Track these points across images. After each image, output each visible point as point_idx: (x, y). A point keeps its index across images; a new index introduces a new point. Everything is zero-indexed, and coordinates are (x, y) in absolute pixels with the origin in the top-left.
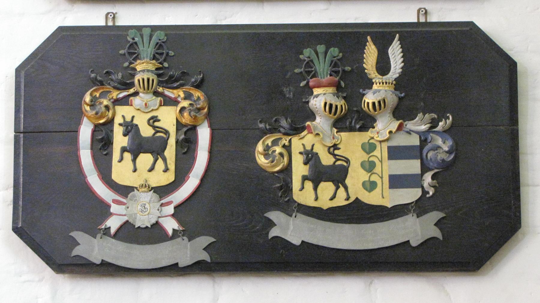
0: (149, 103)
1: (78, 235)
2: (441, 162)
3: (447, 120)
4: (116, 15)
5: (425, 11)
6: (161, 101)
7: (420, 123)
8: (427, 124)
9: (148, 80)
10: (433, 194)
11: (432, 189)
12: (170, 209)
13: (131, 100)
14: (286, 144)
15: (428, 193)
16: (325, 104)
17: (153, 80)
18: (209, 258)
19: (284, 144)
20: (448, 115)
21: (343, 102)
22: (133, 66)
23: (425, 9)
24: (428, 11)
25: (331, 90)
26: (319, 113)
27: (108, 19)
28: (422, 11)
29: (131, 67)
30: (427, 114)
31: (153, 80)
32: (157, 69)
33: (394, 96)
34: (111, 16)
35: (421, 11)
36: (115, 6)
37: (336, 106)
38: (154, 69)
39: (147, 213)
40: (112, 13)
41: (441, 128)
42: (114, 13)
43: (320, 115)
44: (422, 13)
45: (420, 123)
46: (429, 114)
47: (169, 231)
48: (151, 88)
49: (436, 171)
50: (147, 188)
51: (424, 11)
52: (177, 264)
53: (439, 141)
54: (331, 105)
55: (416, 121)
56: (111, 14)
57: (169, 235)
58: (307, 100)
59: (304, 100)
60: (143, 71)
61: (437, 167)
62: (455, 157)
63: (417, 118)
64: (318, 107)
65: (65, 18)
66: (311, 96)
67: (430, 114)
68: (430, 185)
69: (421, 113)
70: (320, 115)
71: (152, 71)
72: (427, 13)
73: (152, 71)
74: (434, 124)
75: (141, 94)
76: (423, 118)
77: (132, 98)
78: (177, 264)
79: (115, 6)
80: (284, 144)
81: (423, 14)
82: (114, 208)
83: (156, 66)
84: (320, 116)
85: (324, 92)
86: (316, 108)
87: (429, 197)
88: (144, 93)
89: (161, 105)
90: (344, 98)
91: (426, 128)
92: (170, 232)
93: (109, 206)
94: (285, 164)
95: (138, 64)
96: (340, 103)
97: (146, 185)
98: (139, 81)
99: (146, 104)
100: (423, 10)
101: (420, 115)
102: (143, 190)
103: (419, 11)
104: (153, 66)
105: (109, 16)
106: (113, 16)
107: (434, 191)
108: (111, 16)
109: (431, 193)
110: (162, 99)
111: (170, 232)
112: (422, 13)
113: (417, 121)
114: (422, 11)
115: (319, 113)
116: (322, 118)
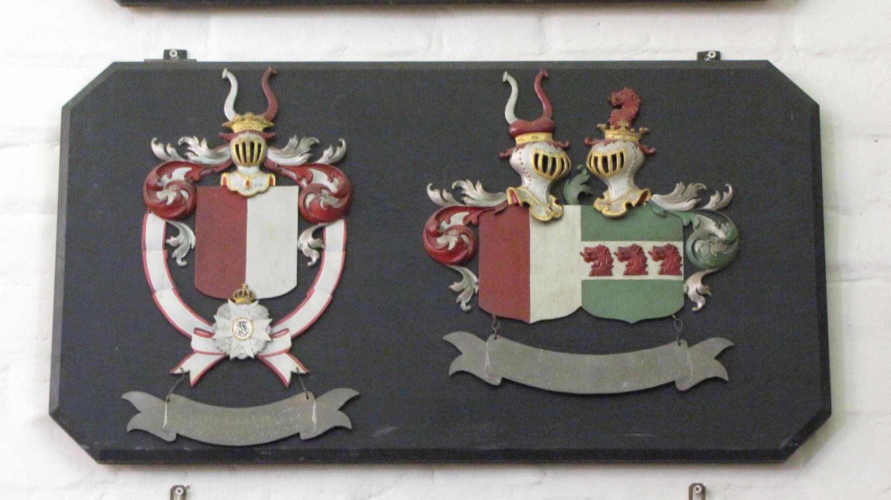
0: (253, 182)
1: (136, 397)
2: (716, 256)
3: (725, 194)
4: (188, 491)
5: (702, 488)
6: (271, 180)
7: (293, 152)
8: (691, 199)
9: (252, 145)
10: (704, 307)
11: (703, 298)
12: (285, 342)
13: (225, 179)
14: (472, 222)
15: (695, 304)
16: (537, 156)
17: (259, 146)
18: (350, 424)
19: (470, 222)
20: (727, 185)
21: (563, 155)
22: (228, 126)
23: (701, 485)
24: (706, 489)
25: (542, 136)
26: (527, 173)
27: (174, 496)
28: (697, 489)
29: (224, 127)
30: (691, 184)
31: (259, 146)
32: (266, 130)
33: (638, 150)
34: (179, 491)
35: (695, 489)
36: (187, 475)
37: (554, 160)
38: (260, 129)
39: (248, 336)
40: (182, 487)
41: (714, 204)
42: (185, 486)
43: (528, 174)
44: (697, 492)
45: (293, 152)
46: (692, 185)
47: (285, 377)
48: (255, 160)
49: (708, 271)
50: (248, 296)
51: (700, 490)
52: (298, 435)
53: (711, 226)
54: (545, 159)
55: (674, 195)
56: (179, 489)
57: (287, 382)
58: (506, 154)
59: (502, 155)
60: (243, 132)
61: (710, 264)
62: (738, 253)
63: (675, 191)
64: (524, 163)
65: (103, 495)
66: (512, 149)
67: (695, 183)
68: (698, 292)
69: (681, 183)
70: (528, 174)
71: (259, 133)
72: (705, 493)
73: (259, 133)
74: (703, 197)
75: (240, 168)
76: (685, 190)
77: (224, 175)
78: (298, 435)
79: (187, 475)
80: (470, 222)
81: (697, 494)
82: (197, 343)
83: (265, 124)
84: (529, 176)
85: (534, 140)
86: (522, 164)
87: (696, 312)
88: (244, 166)
89: (271, 185)
90: (565, 149)
91: (690, 206)
92: (287, 377)
93: (188, 339)
94: (470, 251)
95: (236, 121)
96: (559, 155)
97: (246, 292)
98: (237, 147)
99: (248, 183)
100: (698, 486)
101: (679, 187)
102: (242, 299)
103: (691, 488)
104: (260, 125)
105: (176, 491)
106: (182, 491)
107: (704, 302)
108: (179, 491)
109: (700, 305)
110: (274, 177)
111: (287, 377)
112: (697, 492)
113: (676, 195)
114: (697, 489)
115: (527, 173)
116: (532, 180)
